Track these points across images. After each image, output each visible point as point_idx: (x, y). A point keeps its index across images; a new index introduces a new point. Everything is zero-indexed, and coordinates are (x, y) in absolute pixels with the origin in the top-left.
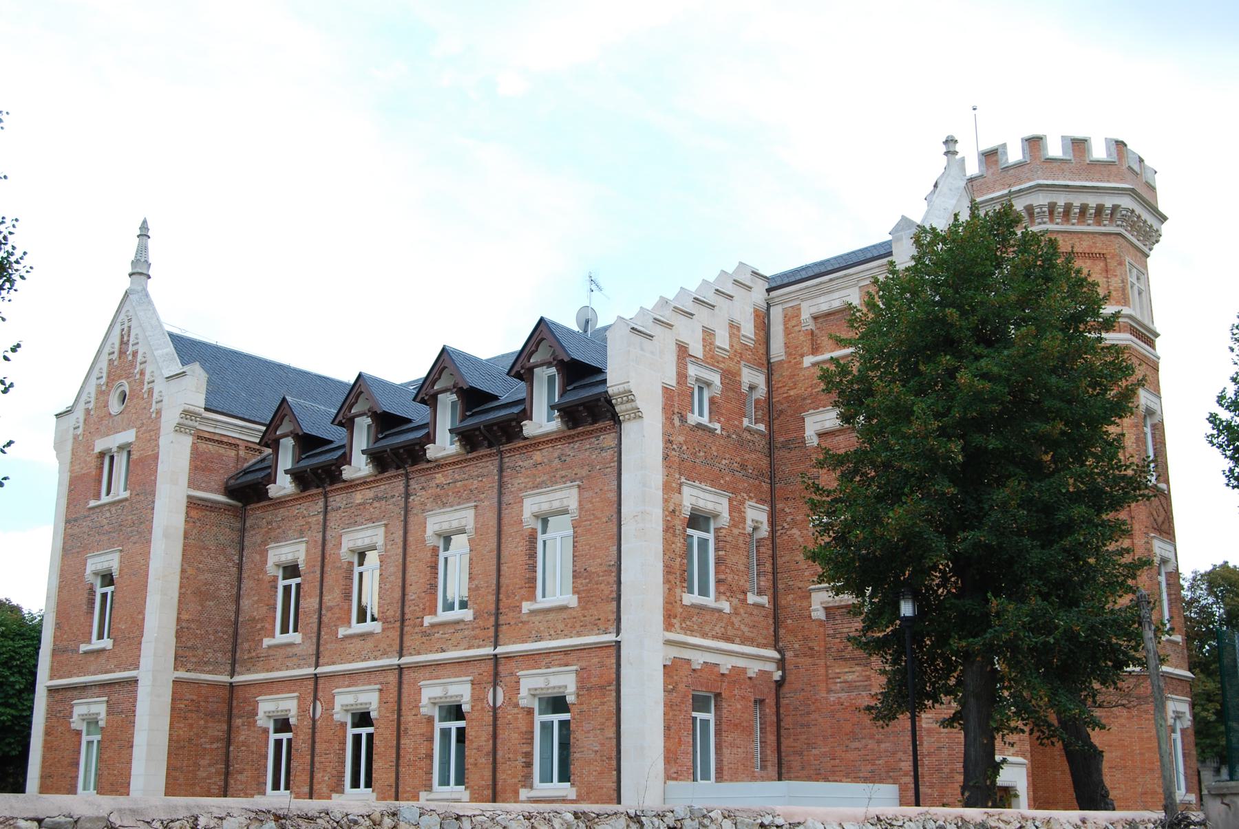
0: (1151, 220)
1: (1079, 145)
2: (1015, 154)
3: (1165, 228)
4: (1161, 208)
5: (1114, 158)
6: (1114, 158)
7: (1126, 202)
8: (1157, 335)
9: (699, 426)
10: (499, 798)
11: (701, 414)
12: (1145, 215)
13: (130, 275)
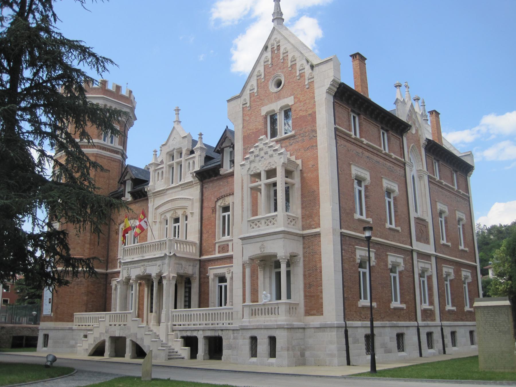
1: (118, 88)
5: (128, 96)
6: (128, 96)
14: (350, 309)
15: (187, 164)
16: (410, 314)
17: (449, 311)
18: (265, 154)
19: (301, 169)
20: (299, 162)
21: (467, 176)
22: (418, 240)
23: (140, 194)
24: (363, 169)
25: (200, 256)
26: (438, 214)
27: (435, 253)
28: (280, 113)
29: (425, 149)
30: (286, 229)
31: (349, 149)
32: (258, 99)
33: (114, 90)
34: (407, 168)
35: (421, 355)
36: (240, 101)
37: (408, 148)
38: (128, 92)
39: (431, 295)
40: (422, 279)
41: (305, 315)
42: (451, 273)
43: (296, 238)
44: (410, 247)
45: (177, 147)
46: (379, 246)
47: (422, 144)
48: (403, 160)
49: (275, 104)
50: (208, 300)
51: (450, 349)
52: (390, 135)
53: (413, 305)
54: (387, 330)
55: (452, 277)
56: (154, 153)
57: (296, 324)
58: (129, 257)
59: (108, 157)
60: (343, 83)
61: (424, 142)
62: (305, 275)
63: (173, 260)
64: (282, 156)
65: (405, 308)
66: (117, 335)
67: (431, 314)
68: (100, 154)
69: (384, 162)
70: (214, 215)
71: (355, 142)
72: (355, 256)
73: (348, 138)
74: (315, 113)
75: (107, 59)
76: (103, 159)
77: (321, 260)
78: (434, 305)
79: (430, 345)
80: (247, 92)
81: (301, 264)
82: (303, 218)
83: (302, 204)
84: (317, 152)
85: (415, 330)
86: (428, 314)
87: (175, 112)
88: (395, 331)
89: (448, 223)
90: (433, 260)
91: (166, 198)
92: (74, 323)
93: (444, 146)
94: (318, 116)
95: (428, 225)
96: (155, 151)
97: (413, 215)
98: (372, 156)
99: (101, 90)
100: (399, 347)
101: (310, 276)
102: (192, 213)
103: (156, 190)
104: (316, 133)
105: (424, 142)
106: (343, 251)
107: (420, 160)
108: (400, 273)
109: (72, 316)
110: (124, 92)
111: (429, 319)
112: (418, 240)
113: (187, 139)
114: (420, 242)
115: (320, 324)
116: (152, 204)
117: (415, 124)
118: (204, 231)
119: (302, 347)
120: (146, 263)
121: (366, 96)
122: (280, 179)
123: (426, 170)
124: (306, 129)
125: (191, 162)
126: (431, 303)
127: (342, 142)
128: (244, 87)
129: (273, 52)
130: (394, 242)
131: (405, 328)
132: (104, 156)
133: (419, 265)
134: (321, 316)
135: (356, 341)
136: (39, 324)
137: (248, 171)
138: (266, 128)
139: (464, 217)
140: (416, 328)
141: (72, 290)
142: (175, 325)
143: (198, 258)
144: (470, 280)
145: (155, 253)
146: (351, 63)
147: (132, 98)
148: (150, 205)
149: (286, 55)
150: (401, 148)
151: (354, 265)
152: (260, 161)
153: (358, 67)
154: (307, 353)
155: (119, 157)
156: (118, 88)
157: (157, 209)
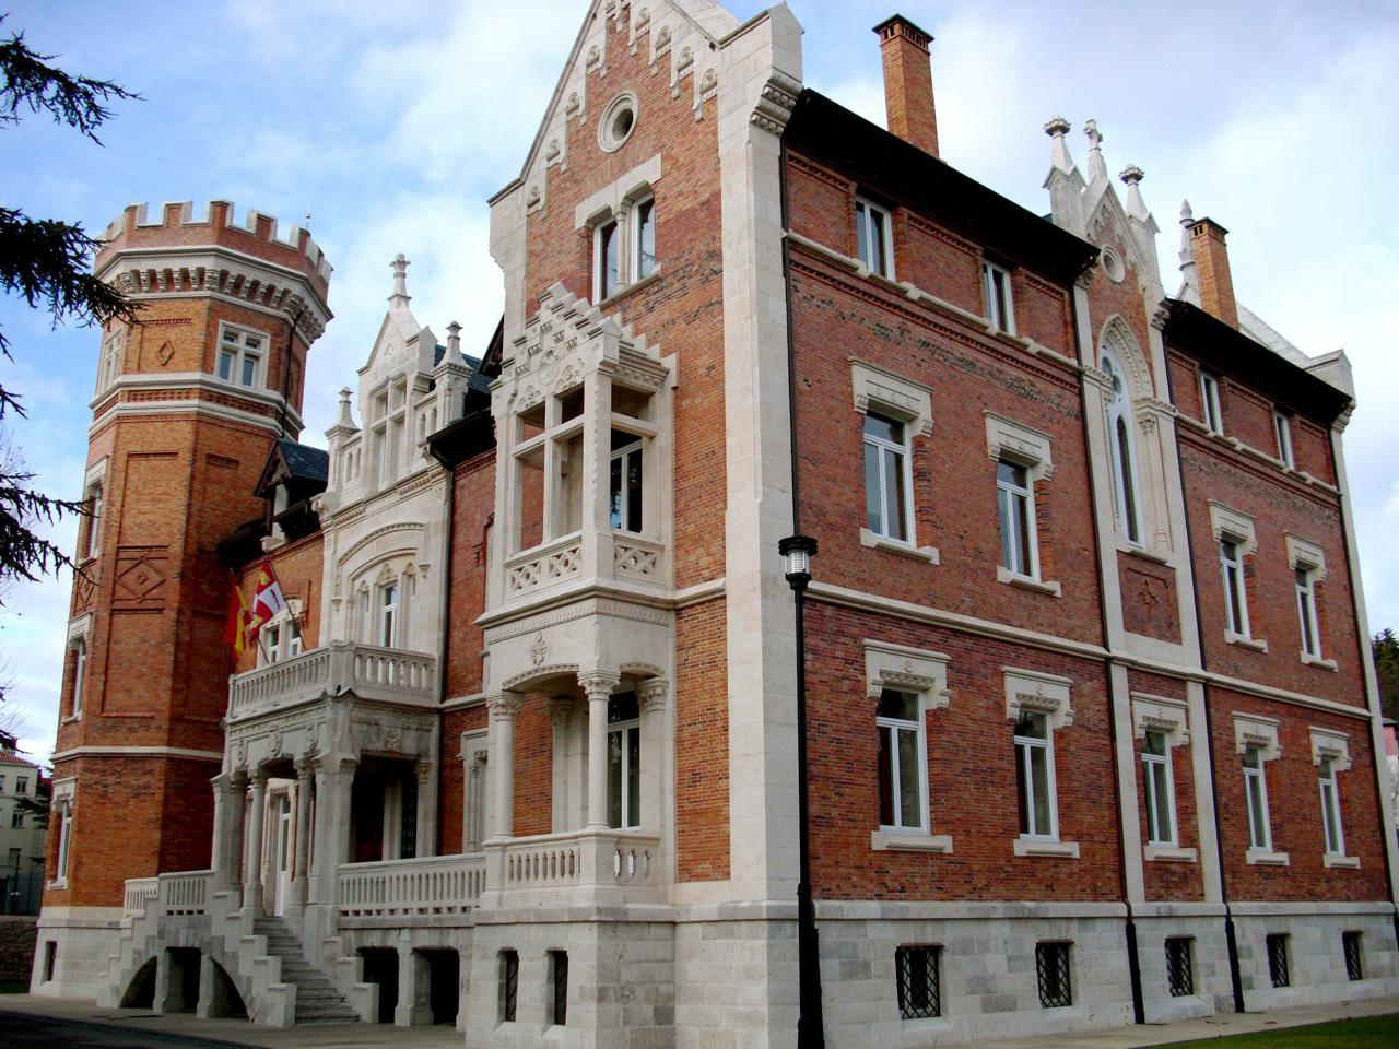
0: (317, 314)
1: (265, 222)
2: (155, 217)
3: (330, 326)
4: (330, 304)
5: (295, 244)
6: (295, 244)
7: (296, 289)
8: (302, 427)
9: (1312, 665)
10: (445, 850)
11: (1238, 629)
12: (312, 307)
13: (1182, 268)
14: (825, 853)
15: (418, 422)
16: (1101, 874)
17: (1262, 868)
18: (558, 340)
19: (674, 385)
20: (670, 362)
21: (1329, 429)
22: (1132, 624)
23: (304, 527)
24: (903, 380)
25: (444, 696)
26: (1210, 548)
27: (1200, 671)
28: (624, 214)
29: (1164, 333)
30: (606, 583)
31: (847, 313)
32: (568, 179)
33: (253, 230)
34: (1091, 392)
35: (1140, 1017)
36: (522, 196)
37: (1096, 324)
39: (1187, 813)
40: (1150, 759)
41: (679, 880)
42: (1341, 751)
43: (650, 613)
44: (1102, 651)
45: (393, 373)
46: (970, 643)
47: (1150, 317)
48: (1074, 362)
49: (611, 187)
50: (459, 833)
51: (1262, 995)
52: (1022, 279)
53: (1111, 845)
54: (997, 931)
55: (1273, 752)
56: (341, 398)
57: (639, 907)
58: (245, 707)
60: (810, 92)
61: (1158, 309)
62: (679, 742)
63: (343, 713)
64: (599, 340)
65: (1077, 855)
66: (182, 944)
67: (1185, 877)
68: (208, 416)
69: (996, 365)
70: (481, 569)
71: (873, 291)
72: (864, 673)
73: (842, 277)
74: (717, 195)
75: (101, 85)
76: (218, 429)
77: (725, 687)
78: (1198, 847)
79: (1181, 980)
80: (542, 164)
81: (670, 704)
82: (677, 547)
83: (676, 501)
84: (722, 321)
85: (1119, 930)
86: (1171, 879)
87: (393, 270)
88: (1030, 938)
89: (1258, 574)
90: (1196, 693)
91: (366, 528)
92: (125, 910)
93: (1242, 332)
94: (727, 204)
95: (1174, 578)
96: (347, 393)
97: (1113, 539)
98: (945, 341)
99: (209, 231)
100: (1275, 976)
102: (425, 568)
103: (343, 506)
104: (721, 261)
105: (1158, 309)
106: (808, 656)
107: (1144, 366)
108: (1059, 735)
109: (120, 888)
110: (284, 234)
111: (1180, 894)
112: (1132, 624)
113: (417, 345)
114: (1144, 633)
115: (721, 910)
116: (332, 550)
117: (1123, 253)
118: (456, 620)
119: (663, 989)
120: (280, 723)
121: (929, 151)
122: (595, 420)
123: (1168, 401)
124: (694, 252)
125: (429, 413)
126: (1189, 839)
127: (809, 287)
128: (534, 151)
129: (611, 30)
130: (1033, 629)
131: (1074, 925)
132: (222, 420)
133: (1133, 712)
134: (726, 883)
135: (857, 969)
136: (37, 913)
137: (511, 402)
138: (590, 266)
139: (1319, 559)
140: (1123, 924)
141: (120, 812)
142: (346, 913)
143: (435, 703)
144: (1343, 763)
145: (304, 690)
146: (879, 52)
147: (310, 252)
148: (327, 553)
149: (644, 29)
150: (1066, 324)
151: (856, 704)
152: (543, 365)
153: (900, 61)
155: (270, 422)
156: (265, 222)
157: (342, 561)
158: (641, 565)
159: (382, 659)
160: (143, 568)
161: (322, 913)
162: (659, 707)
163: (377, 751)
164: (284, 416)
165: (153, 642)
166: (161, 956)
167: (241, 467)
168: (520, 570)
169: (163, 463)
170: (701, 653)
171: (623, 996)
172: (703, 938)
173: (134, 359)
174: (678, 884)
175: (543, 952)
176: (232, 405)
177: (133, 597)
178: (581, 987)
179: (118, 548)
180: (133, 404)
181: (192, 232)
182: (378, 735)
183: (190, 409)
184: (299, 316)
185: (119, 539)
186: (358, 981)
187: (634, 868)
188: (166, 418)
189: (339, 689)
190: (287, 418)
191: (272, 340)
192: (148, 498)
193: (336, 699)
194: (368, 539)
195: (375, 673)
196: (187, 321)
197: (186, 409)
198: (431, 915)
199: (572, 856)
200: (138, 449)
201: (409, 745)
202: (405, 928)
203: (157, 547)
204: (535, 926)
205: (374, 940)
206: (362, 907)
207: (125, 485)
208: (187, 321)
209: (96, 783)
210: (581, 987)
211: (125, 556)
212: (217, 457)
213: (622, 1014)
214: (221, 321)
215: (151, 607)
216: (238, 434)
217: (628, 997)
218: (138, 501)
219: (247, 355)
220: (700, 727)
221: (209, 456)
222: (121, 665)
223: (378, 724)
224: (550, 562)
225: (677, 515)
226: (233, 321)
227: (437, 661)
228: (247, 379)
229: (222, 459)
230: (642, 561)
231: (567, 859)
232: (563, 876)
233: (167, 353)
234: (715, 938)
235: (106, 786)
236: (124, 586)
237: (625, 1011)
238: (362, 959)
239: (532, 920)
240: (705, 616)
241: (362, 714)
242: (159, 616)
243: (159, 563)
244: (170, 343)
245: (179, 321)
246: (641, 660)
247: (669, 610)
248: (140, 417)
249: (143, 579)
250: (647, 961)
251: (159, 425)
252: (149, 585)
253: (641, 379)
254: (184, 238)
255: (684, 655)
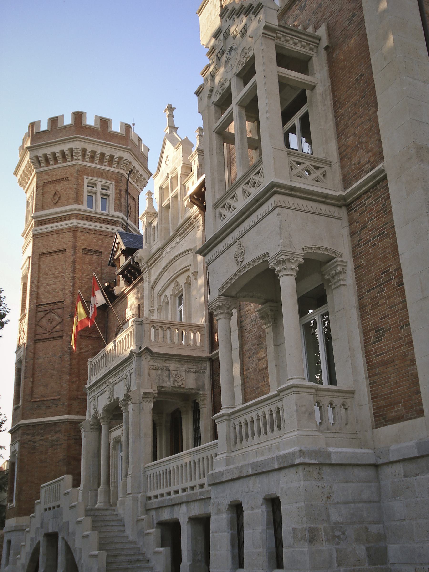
2: (44, 127)
6: (124, 133)
33: (98, 126)
38: (124, 128)
59: (96, 230)
62: (361, 308)
66: (50, 531)
76: (88, 235)
81: (349, 279)
82: (341, 159)
91: (163, 263)
99: (74, 128)
101: (374, 307)
119: (374, 529)
137: (210, 96)
142: (150, 498)
154: (393, 550)
158: (313, 176)
159: (169, 328)
160: (51, 315)
161: (135, 500)
162: (342, 282)
163: (169, 388)
164: (127, 227)
165: (58, 356)
166: (41, 538)
167: (103, 255)
168: (224, 206)
169: (59, 256)
170: (372, 230)
171: (334, 537)
172: (405, 476)
173: (40, 204)
174: (375, 430)
175: (260, 500)
176: (95, 221)
177: (45, 332)
178: (294, 529)
179: (37, 306)
180: (40, 227)
181: (64, 131)
182: (169, 377)
183: (71, 225)
184: (130, 173)
185: (37, 300)
186: (157, 547)
187: (334, 417)
188: (58, 232)
189: (140, 348)
190: (129, 227)
191: (115, 185)
192: (51, 276)
193: (139, 355)
194: (165, 269)
195: (164, 337)
196: (67, 179)
197: (69, 225)
198: (197, 490)
199: (278, 412)
200: (45, 251)
201: (190, 382)
202: (183, 503)
203: (58, 302)
204: (253, 478)
205: (166, 515)
206: (158, 492)
207: (39, 271)
208: (67, 179)
209: (29, 441)
210: (294, 529)
211: (41, 310)
212: (89, 250)
213: (335, 554)
214: (85, 177)
215: (56, 336)
216: (100, 237)
217: (339, 537)
218: (46, 279)
219: (102, 194)
220: (378, 289)
221: (84, 250)
222: (41, 371)
223: (169, 370)
224: (243, 189)
225: (339, 136)
226: (92, 176)
227: (206, 327)
228: (104, 208)
229: (92, 251)
230: (314, 173)
231: (275, 414)
232: (273, 431)
233: (57, 198)
234: (417, 475)
235: (35, 442)
236: (41, 327)
237: (337, 551)
238: (159, 530)
239: (250, 473)
240: (371, 200)
241: (157, 364)
242: (60, 340)
243: (59, 311)
244: (58, 192)
245: (61, 180)
246: (320, 244)
247: (340, 207)
248: (44, 233)
249: (50, 321)
250: (354, 502)
251: (55, 236)
252: (54, 324)
253: (299, 45)
254: (61, 135)
255: (357, 237)
